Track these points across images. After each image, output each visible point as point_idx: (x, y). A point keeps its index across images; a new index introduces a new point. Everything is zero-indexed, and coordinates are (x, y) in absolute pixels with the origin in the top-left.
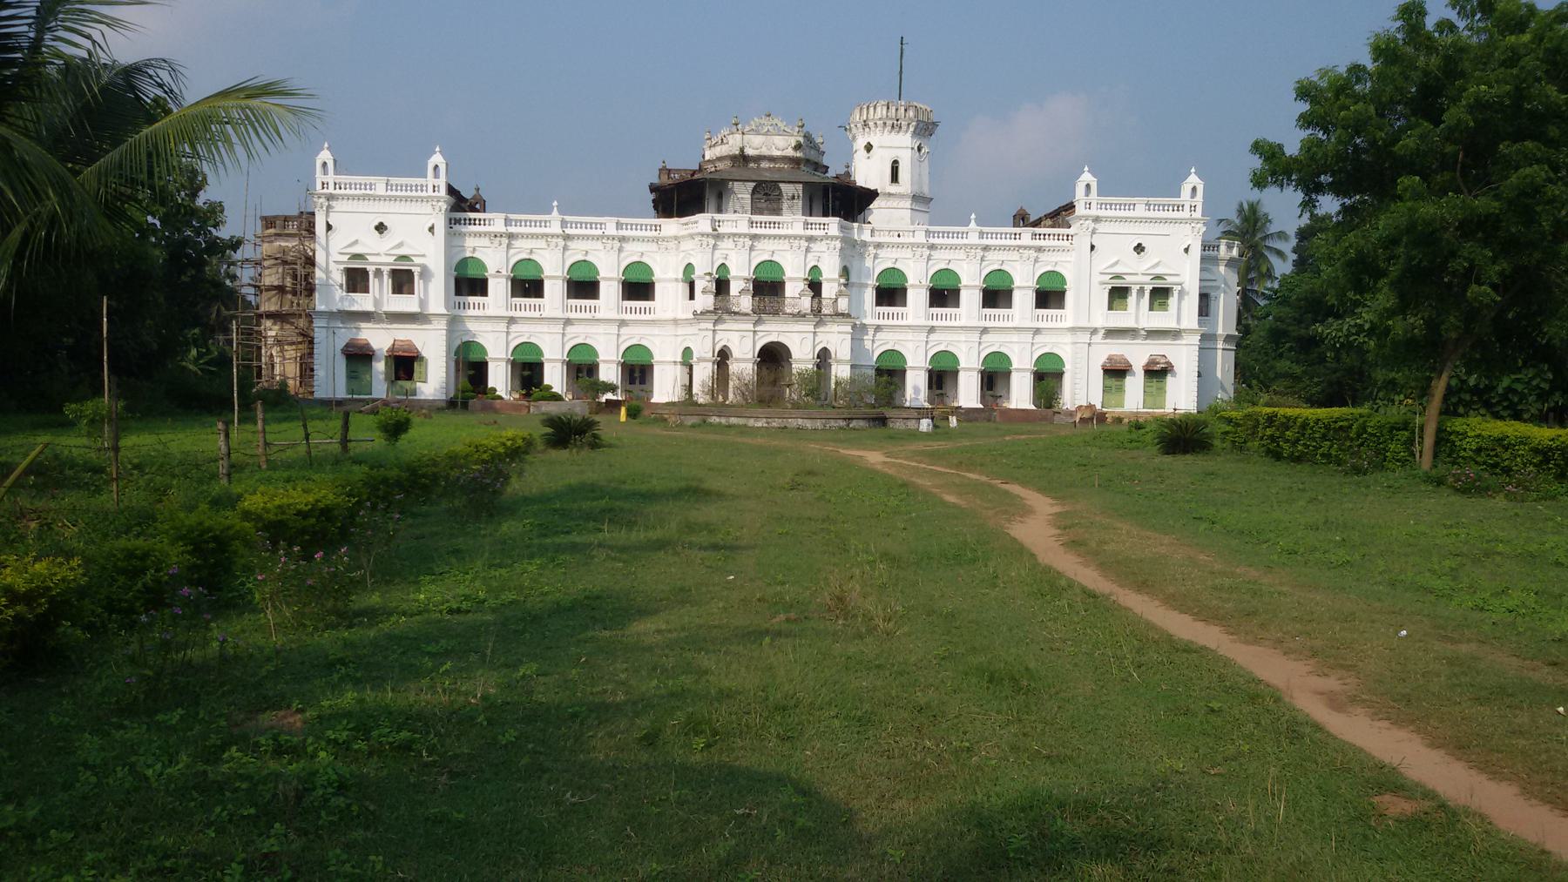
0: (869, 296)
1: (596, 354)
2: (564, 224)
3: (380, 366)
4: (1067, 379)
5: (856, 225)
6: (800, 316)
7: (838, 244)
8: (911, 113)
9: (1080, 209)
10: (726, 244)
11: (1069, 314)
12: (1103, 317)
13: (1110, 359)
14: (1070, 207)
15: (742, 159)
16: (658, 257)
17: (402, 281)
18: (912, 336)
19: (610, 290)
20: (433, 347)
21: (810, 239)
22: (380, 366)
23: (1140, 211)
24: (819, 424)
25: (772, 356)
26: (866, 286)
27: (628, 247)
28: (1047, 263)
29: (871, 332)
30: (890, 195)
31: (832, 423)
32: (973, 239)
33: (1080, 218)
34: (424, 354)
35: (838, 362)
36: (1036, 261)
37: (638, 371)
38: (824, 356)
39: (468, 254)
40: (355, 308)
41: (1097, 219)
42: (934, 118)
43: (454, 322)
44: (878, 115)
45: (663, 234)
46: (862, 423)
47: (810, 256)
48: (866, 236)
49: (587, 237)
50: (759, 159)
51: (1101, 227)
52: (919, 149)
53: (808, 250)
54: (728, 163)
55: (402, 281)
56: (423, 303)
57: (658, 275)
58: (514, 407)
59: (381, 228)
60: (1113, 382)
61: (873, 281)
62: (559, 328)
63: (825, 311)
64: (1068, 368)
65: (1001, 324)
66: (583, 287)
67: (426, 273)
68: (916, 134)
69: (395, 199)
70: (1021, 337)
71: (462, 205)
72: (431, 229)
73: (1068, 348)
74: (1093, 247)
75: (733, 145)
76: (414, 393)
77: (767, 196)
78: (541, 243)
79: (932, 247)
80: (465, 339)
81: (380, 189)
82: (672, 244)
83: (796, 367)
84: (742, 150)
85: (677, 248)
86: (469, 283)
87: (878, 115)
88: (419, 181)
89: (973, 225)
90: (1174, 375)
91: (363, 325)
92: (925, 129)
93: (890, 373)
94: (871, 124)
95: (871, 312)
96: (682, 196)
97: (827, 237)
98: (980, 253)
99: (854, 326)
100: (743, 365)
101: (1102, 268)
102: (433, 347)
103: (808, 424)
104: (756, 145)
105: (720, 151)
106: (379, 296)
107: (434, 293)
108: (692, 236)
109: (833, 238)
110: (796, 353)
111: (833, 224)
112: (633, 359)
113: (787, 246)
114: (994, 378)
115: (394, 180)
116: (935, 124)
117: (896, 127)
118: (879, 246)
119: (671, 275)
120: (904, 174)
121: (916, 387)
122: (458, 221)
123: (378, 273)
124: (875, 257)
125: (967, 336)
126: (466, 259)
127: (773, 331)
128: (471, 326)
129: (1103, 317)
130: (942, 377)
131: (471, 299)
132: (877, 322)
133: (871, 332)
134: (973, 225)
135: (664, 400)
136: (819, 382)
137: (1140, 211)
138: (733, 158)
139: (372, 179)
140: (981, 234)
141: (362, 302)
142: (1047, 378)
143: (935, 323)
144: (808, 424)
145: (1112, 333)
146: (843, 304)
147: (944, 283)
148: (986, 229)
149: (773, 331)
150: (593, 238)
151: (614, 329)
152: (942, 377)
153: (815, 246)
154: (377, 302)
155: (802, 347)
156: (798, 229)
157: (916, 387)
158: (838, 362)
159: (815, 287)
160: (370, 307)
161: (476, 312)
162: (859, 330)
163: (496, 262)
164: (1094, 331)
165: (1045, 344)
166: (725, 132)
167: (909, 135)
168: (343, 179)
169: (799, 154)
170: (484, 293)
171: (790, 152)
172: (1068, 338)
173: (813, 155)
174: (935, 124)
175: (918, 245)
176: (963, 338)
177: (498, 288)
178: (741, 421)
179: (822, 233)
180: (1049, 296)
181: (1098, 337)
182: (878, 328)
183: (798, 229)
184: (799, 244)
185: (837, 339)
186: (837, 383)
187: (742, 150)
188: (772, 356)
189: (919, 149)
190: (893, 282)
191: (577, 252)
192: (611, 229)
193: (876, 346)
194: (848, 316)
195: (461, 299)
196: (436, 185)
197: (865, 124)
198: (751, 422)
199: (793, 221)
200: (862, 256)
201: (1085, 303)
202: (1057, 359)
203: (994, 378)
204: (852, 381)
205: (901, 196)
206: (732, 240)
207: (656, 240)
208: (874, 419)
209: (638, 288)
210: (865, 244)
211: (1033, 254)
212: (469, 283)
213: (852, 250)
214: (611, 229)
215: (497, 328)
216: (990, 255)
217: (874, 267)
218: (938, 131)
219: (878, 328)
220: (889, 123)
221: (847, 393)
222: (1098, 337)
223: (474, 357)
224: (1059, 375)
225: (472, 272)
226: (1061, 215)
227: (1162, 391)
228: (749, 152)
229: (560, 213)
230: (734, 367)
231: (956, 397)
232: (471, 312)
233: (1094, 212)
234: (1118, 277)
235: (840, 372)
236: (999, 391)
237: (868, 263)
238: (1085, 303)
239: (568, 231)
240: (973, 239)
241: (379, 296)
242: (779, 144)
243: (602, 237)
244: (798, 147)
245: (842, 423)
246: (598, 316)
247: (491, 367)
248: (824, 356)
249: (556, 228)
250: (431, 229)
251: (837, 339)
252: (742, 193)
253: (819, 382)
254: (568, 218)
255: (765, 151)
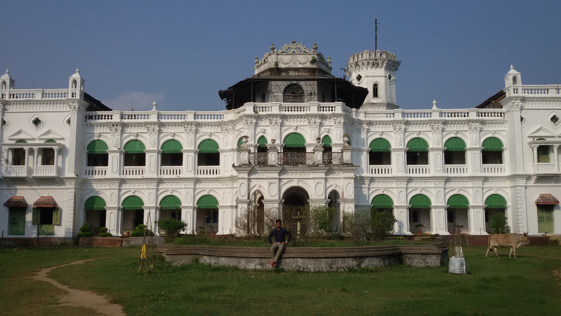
0: (365, 158)
1: (180, 203)
2: (159, 116)
3: (29, 217)
4: (509, 213)
5: (354, 109)
6: (315, 167)
7: (342, 120)
8: (384, 56)
9: (510, 94)
10: (265, 123)
11: (506, 168)
12: (532, 167)
13: (542, 196)
14: (501, 94)
15: (277, 70)
16: (221, 135)
17: (48, 156)
18: (396, 185)
19: (189, 159)
20: (65, 199)
21: (323, 117)
22: (29, 217)
23: (552, 93)
24: (323, 265)
25: (295, 198)
26: (362, 151)
27: (202, 130)
28: (490, 131)
29: (367, 182)
30: (373, 104)
31: (340, 263)
32: (436, 116)
33: (511, 98)
34: (60, 205)
35: (346, 201)
36: (481, 130)
37: (208, 213)
38: (334, 198)
39: (96, 138)
40: (13, 175)
41: (523, 100)
42: (397, 59)
43: (82, 183)
44: (365, 57)
45: (225, 120)
46: (376, 262)
47: (323, 129)
48: (362, 117)
49: (174, 124)
50: (287, 70)
51: (527, 105)
52: (390, 78)
53: (321, 125)
54: (268, 73)
55: (48, 156)
56: (60, 171)
57: (222, 146)
58: (114, 241)
59: (37, 122)
60: (544, 214)
61: (367, 147)
62: (153, 185)
63: (334, 162)
64: (509, 203)
65: (459, 175)
66: (172, 157)
67: (63, 150)
68: (387, 69)
69: (50, 102)
70: (474, 183)
71: (92, 106)
72: (69, 122)
73: (509, 191)
74: (522, 119)
75: (271, 61)
76: (53, 234)
77: (294, 93)
78: (143, 129)
79: (407, 123)
80: (93, 194)
81: (38, 97)
82: (230, 127)
83: (312, 206)
84: (277, 64)
85: (231, 130)
86: (96, 157)
87: (365, 57)
88: (63, 90)
89: (434, 107)
90: (559, 208)
91: (18, 187)
92: (393, 66)
93: (382, 210)
94: (360, 63)
95: (366, 169)
96: (240, 94)
97: (334, 115)
98: (441, 126)
99: (356, 179)
100: (273, 208)
101: (529, 133)
102: (65, 199)
103: (311, 265)
104: (285, 61)
105: (262, 68)
106: (34, 166)
107: (68, 165)
108: (241, 118)
109: (338, 115)
110: (312, 195)
111: (338, 107)
112: (204, 205)
113: (306, 123)
114: (457, 211)
115: (47, 91)
116: (398, 63)
117: (375, 65)
118: (370, 123)
119: (229, 147)
120: (381, 91)
121: (402, 224)
122: (91, 117)
123: (31, 151)
124: (368, 131)
125: (435, 184)
126: (94, 141)
127: (295, 179)
128: (96, 186)
129: (532, 167)
130: (419, 212)
131: (97, 168)
132: (370, 175)
133: (367, 182)
134: (434, 107)
135: (227, 232)
136: (331, 217)
137: (552, 93)
138: (270, 70)
139: (31, 91)
140: (441, 114)
141: (20, 171)
142: (495, 212)
143: (412, 175)
144: (311, 265)
145: (542, 178)
146: (347, 156)
147: (417, 147)
148: (444, 110)
149: (295, 179)
150: (178, 124)
151: (191, 185)
152: (419, 212)
153: (327, 123)
154: (30, 171)
155: (316, 189)
156: (314, 110)
157: (402, 224)
158: (346, 201)
159: (327, 149)
160: (24, 174)
161: (96, 177)
162: (359, 181)
163: (113, 142)
164: (529, 177)
165: (492, 188)
166: (265, 56)
167: (383, 69)
168: (13, 91)
169: (314, 66)
170: (106, 164)
171: (309, 65)
172: (508, 184)
173: (324, 67)
174: (398, 63)
175: (398, 122)
176: (432, 185)
177: (115, 159)
178: (232, 262)
179: (331, 112)
180: (492, 154)
181: (532, 182)
182: (372, 180)
183: (314, 110)
184: (316, 123)
185: (343, 183)
186: (345, 218)
187: (277, 64)
188: (295, 198)
189: (390, 78)
190: (380, 148)
191: (168, 134)
192: (190, 118)
193: (371, 192)
194: (351, 165)
195: (91, 168)
196: (74, 91)
197: (357, 64)
198: (243, 264)
199: (312, 107)
200: (359, 131)
201: (520, 159)
202: (501, 198)
203: (457, 211)
204: (357, 215)
205: (380, 104)
206: (270, 122)
207: (219, 124)
208: (389, 257)
209: (209, 157)
210: (360, 122)
211: (478, 125)
212: (96, 157)
213: (352, 128)
214: (190, 118)
215: (112, 187)
216: (448, 128)
217: (368, 138)
218: (400, 67)
219: (372, 180)
220: (371, 62)
221: (352, 225)
222: (532, 182)
223: (97, 206)
224: (503, 210)
225: (98, 150)
226: (496, 100)
227: (551, 220)
228: (282, 66)
229: (157, 109)
230: (267, 206)
231: (429, 228)
232: (96, 177)
233: (520, 94)
234: (541, 138)
235: (347, 208)
236: (422, 221)
237: (363, 135)
238: (520, 159)
239: (163, 121)
240: (436, 116)
241: (34, 166)
242: (303, 61)
243: (184, 123)
244: (313, 61)
245: (352, 263)
246: (181, 176)
247: (108, 213)
248: (334, 198)
249: (153, 118)
250: (69, 122)
251: (343, 183)
252: (277, 88)
253: (331, 217)
254: (162, 112)
255: (292, 65)
